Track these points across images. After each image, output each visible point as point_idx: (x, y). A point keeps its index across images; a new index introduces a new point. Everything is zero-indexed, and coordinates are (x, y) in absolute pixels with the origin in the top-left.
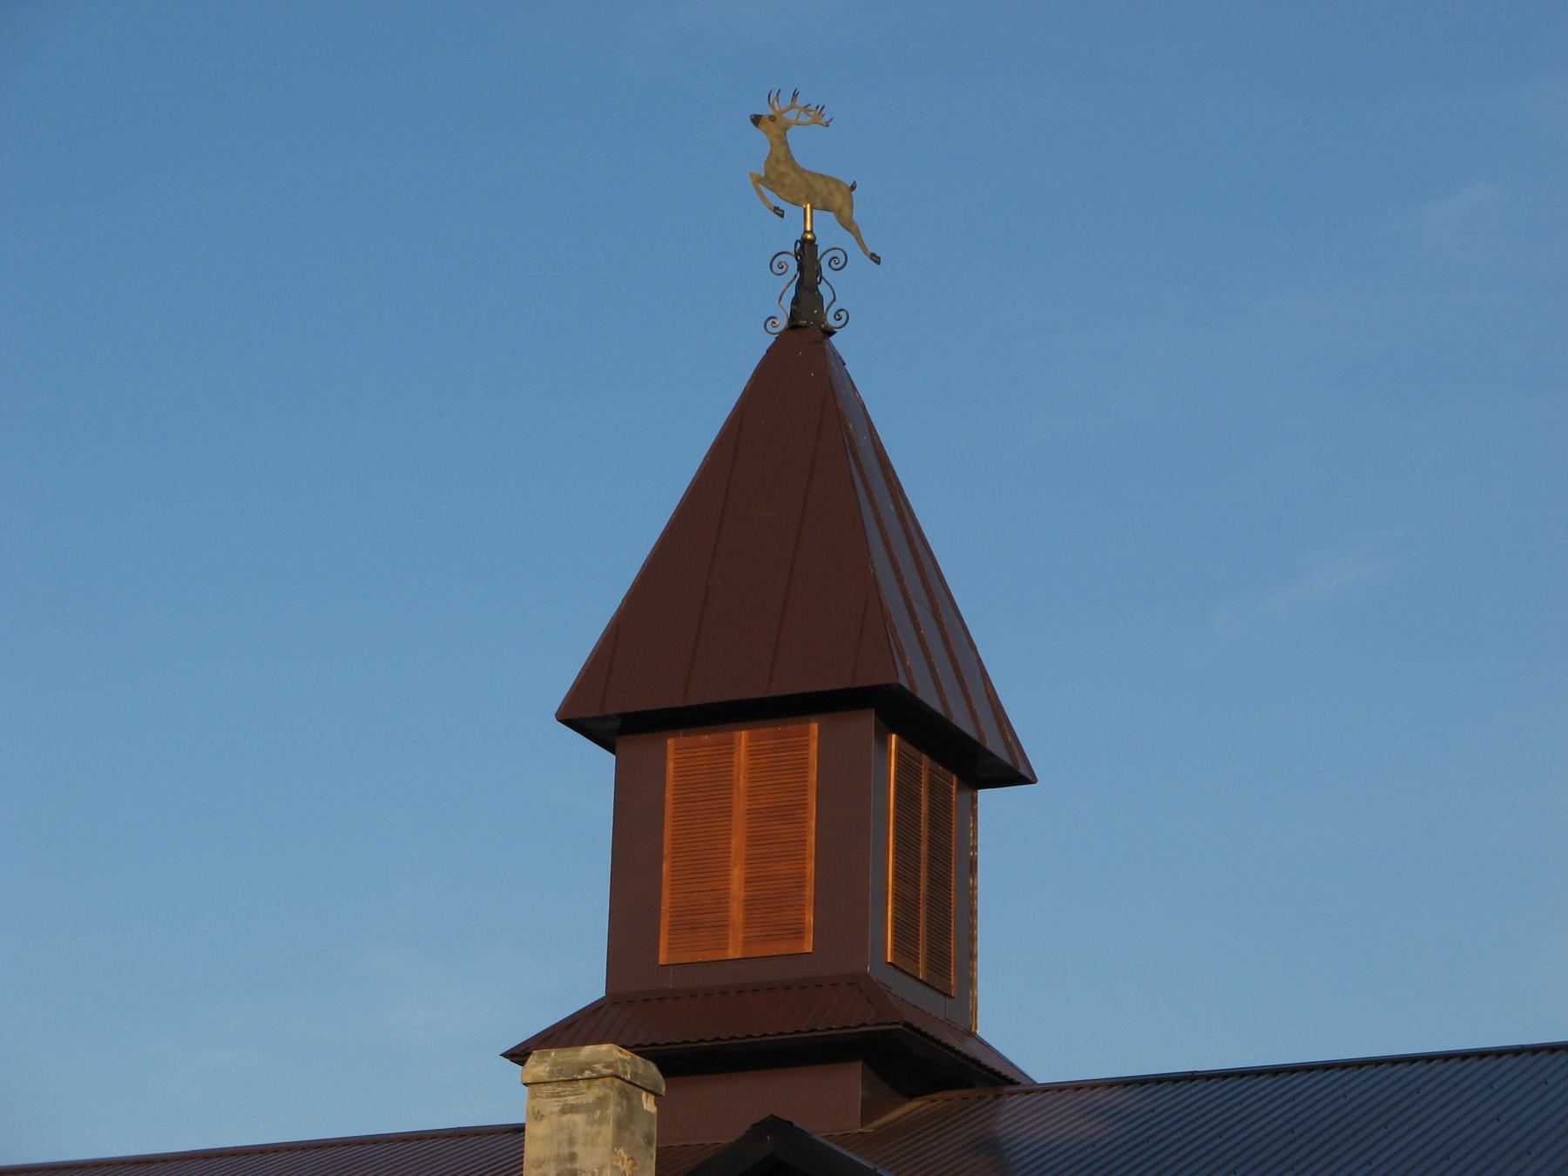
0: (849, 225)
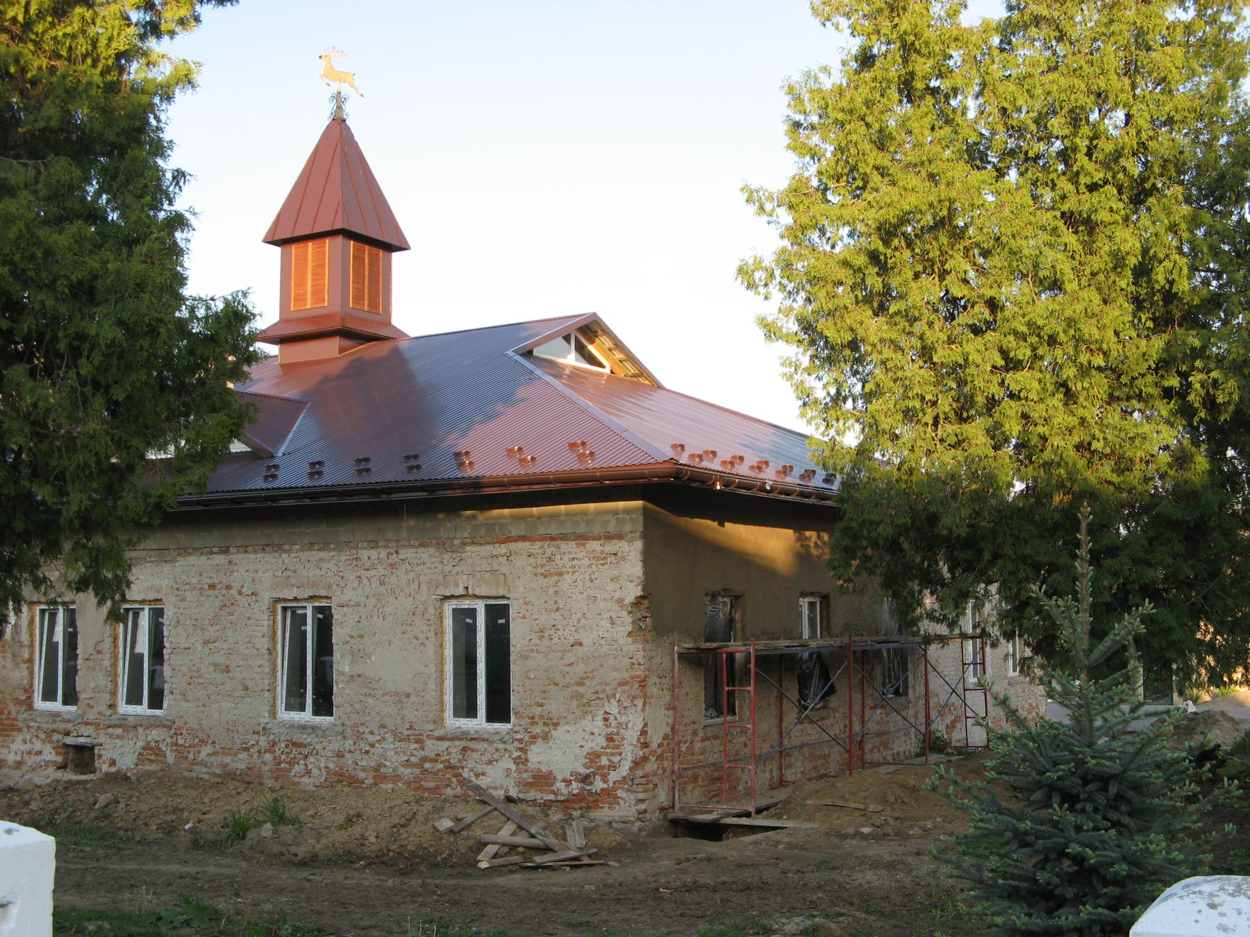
0: (353, 86)
